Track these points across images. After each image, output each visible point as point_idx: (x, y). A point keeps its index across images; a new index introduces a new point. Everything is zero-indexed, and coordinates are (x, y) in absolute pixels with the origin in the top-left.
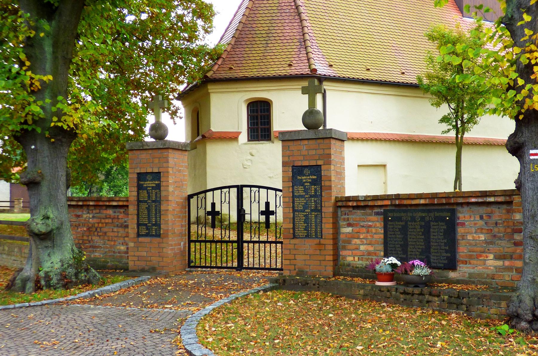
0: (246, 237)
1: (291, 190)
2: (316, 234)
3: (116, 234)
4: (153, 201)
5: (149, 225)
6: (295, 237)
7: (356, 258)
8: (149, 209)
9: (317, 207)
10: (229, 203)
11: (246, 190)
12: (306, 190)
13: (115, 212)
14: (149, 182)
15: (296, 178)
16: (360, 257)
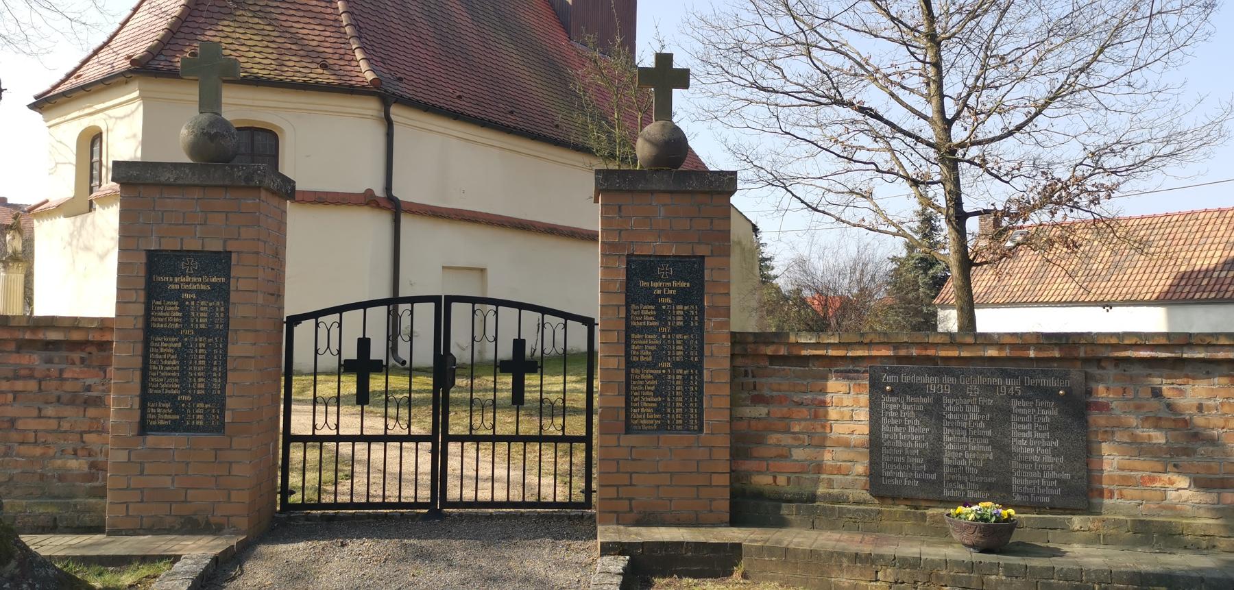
0: (458, 423)
1: (623, 315)
2: (686, 419)
3: (53, 424)
4: (200, 332)
5: (184, 398)
6: (629, 429)
7: (782, 480)
8: (184, 356)
9: (689, 357)
10: (496, 339)
11: (460, 312)
12: (661, 315)
13: (49, 361)
14: (187, 279)
15: (637, 285)
16: (793, 477)
